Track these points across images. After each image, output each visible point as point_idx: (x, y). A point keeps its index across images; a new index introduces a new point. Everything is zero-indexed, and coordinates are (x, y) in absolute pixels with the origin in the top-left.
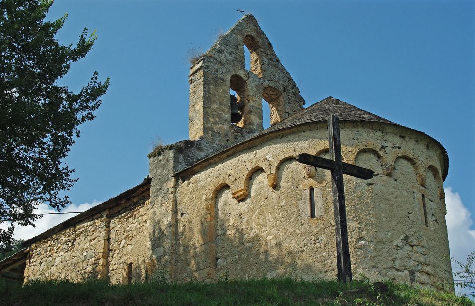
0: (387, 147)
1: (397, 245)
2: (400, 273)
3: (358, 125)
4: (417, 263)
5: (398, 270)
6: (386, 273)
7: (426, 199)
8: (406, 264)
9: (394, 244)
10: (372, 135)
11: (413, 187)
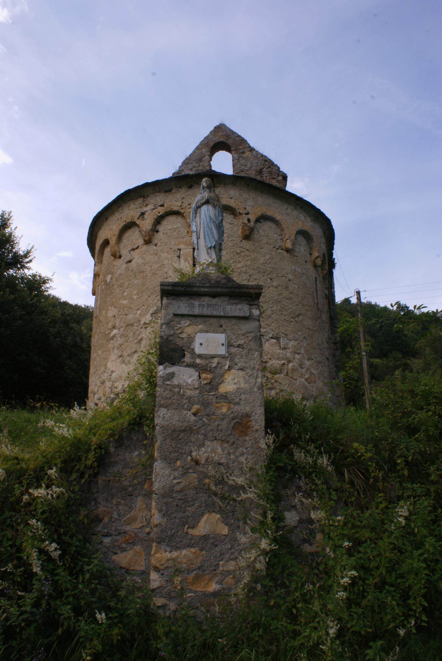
1: (145, 323)
9: (142, 323)
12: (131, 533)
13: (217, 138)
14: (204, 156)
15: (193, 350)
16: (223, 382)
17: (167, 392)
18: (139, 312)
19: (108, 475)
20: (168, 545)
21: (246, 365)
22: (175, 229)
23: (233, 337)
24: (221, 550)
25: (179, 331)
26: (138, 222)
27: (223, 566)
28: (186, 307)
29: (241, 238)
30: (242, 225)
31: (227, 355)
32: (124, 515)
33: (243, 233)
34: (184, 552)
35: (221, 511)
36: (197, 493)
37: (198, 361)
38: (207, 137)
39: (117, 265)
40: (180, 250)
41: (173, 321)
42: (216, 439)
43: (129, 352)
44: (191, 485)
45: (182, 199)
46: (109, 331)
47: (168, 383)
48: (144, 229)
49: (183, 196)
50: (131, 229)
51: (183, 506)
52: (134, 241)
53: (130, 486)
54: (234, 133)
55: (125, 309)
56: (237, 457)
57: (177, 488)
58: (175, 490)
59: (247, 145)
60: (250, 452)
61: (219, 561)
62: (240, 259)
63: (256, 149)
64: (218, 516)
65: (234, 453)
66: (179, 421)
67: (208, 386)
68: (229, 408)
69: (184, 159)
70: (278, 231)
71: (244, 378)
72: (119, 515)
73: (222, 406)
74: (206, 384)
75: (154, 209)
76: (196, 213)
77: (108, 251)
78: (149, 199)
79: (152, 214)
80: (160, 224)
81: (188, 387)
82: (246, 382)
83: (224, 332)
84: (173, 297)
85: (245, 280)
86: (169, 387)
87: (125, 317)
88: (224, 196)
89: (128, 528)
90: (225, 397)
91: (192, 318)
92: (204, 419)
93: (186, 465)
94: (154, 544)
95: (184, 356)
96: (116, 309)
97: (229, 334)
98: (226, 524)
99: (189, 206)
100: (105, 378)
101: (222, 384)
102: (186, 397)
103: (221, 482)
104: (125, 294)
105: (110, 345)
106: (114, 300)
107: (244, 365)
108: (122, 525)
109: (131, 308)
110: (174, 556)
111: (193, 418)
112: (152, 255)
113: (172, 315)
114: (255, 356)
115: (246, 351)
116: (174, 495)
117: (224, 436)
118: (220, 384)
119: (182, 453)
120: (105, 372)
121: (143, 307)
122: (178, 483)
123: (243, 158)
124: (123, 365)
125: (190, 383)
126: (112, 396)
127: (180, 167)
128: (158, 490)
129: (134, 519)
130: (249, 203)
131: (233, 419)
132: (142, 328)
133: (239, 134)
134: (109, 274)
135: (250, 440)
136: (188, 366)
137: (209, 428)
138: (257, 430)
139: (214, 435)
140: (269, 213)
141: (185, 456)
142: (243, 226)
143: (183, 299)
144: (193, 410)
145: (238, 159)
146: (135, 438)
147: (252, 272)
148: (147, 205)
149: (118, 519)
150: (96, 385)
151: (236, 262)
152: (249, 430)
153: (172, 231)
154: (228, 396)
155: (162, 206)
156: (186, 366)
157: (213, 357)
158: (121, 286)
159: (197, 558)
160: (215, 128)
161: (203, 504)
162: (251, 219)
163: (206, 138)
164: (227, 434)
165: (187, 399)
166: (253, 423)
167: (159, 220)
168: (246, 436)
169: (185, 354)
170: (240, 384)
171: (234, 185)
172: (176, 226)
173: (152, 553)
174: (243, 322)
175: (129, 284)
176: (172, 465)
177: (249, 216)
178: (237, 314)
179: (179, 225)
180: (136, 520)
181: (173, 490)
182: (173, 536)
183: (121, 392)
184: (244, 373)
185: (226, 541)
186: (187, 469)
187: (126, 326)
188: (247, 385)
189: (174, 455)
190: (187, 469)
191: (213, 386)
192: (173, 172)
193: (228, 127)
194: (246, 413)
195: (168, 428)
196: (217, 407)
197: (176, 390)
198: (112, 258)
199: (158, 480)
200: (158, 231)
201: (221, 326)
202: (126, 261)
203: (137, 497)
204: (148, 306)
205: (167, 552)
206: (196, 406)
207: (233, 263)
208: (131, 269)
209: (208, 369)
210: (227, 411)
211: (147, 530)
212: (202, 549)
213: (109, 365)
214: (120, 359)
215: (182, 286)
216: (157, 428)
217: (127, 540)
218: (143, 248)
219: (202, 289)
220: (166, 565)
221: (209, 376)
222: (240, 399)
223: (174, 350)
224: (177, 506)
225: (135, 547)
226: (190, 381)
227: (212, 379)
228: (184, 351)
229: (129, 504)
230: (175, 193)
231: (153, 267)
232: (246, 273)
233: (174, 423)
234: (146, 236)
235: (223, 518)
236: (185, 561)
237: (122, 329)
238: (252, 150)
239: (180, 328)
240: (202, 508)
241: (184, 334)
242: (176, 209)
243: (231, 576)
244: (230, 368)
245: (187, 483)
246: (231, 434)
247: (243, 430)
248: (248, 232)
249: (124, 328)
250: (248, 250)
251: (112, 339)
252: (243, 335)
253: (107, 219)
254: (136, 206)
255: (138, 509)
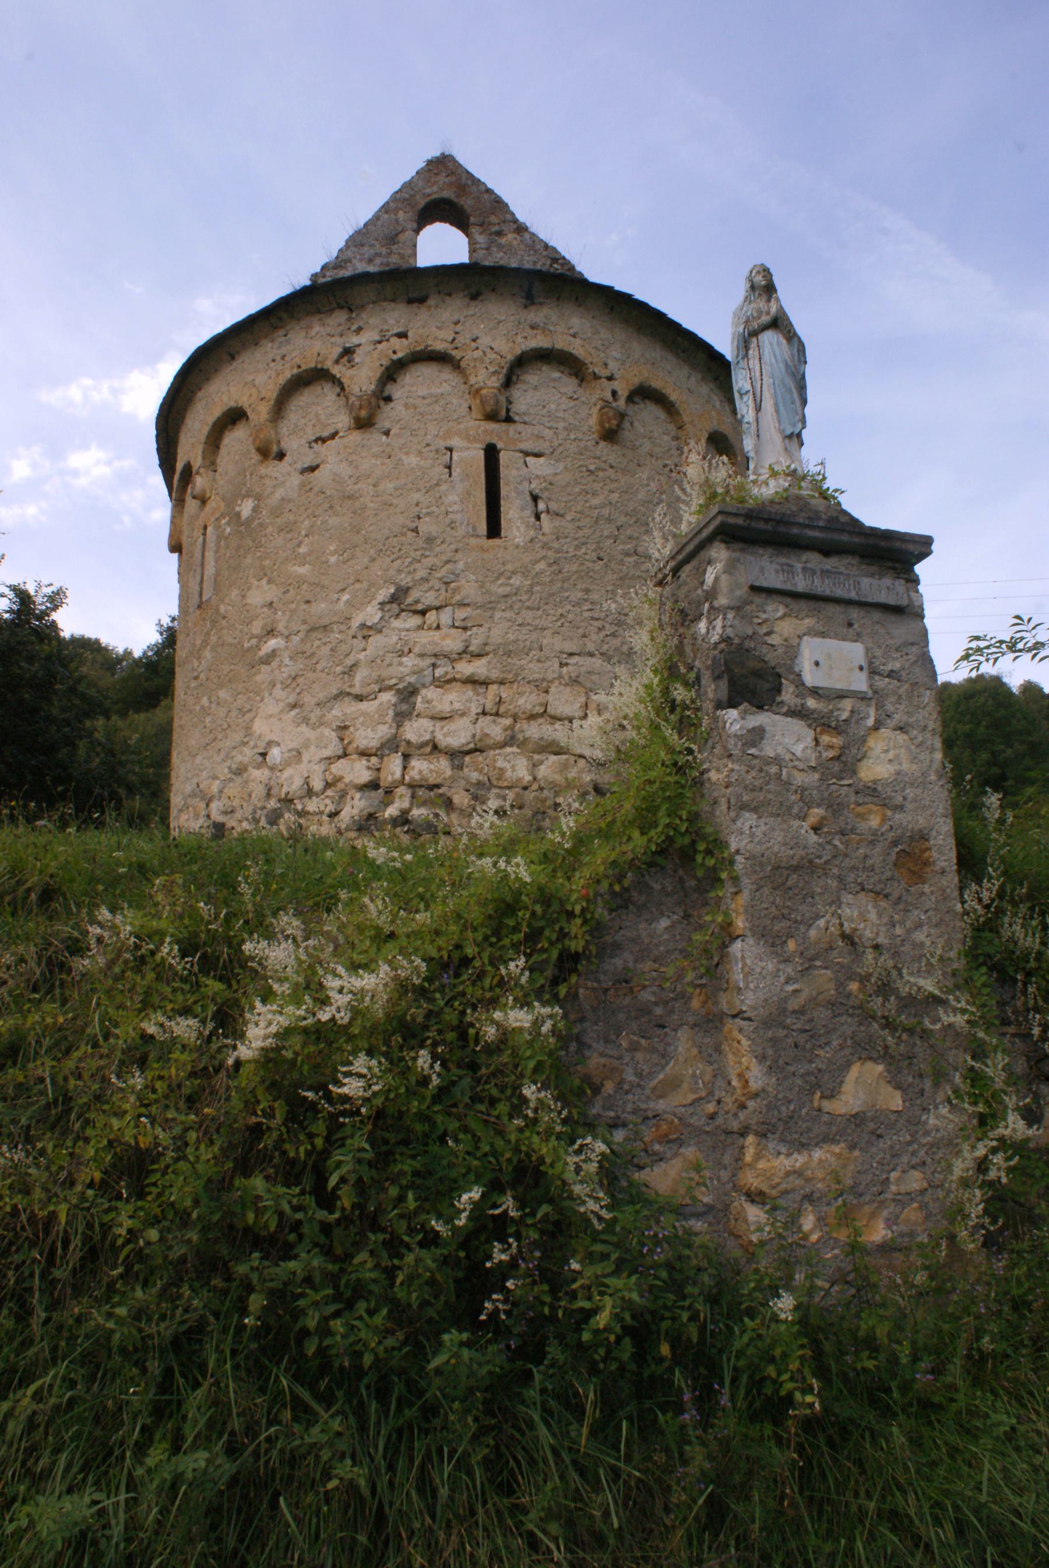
0: (359, 345)
1: (363, 626)
2: (364, 706)
3: (281, 319)
4: (429, 661)
5: (360, 698)
6: (324, 715)
7: (504, 457)
8: (385, 673)
9: (355, 624)
10: (317, 328)
11: (448, 435)
12: (670, 1117)
13: (435, 189)
14: (402, 231)
15: (799, 675)
16: (864, 757)
17: (753, 773)
18: (346, 597)
19: (602, 977)
20: (782, 1140)
21: (911, 720)
22: (437, 398)
23: (878, 653)
24: (891, 1147)
25: (764, 630)
26: (336, 371)
27: (899, 1180)
28: (777, 572)
29: (595, 436)
30: (600, 404)
31: (870, 694)
32: (651, 1075)
33: (601, 423)
34: (817, 1154)
35: (886, 1056)
36: (835, 1016)
37: (811, 703)
38: (410, 182)
39: (274, 475)
40: (450, 450)
41: (751, 603)
42: (863, 889)
43: (321, 696)
44: (821, 997)
45: (457, 323)
46: (254, 641)
47: (752, 751)
48: (356, 390)
49: (456, 318)
50: (311, 388)
51: (808, 1046)
52: (323, 417)
53: (656, 1004)
54: (477, 182)
55: (304, 587)
56: (909, 931)
57: (794, 1004)
58: (790, 1009)
59: (508, 217)
60: (934, 921)
61: (889, 1172)
62: (597, 486)
63: (533, 229)
64: (880, 1068)
65: (902, 922)
66: (785, 844)
67: (837, 763)
68: (884, 819)
69: (351, 232)
70: (672, 427)
71: (907, 748)
72: (639, 1075)
73: (870, 812)
74: (832, 759)
75: (380, 342)
76: (747, 348)
77: (237, 439)
78: (364, 316)
79: (375, 355)
80: (395, 381)
81: (796, 763)
82: (914, 759)
83: (857, 638)
84: (741, 545)
85: (608, 537)
86: (755, 762)
87: (304, 607)
88: (559, 329)
89: (661, 1105)
90: (871, 791)
91: (788, 600)
92: (837, 842)
93: (807, 949)
94: (750, 1139)
95: (779, 690)
96: (274, 587)
97: (870, 645)
98: (898, 1087)
99: (474, 345)
100: (246, 760)
101: (865, 762)
102: (794, 788)
103: (885, 989)
104: (303, 550)
105: (259, 678)
106: (267, 562)
107: (905, 718)
108: (648, 1098)
109: (323, 587)
110: (798, 1164)
111: (813, 838)
112: (375, 456)
113: (746, 589)
114: (926, 700)
115: (906, 686)
116: (788, 1021)
117: (880, 881)
118: (859, 760)
119: (796, 922)
120: (245, 744)
121: (358, 586)
122: (795, 991)
123: (500, 247)
124: (303, 728)
125: (799, 754)
126: (273, 804)
127: (341, 250)
128: (755, 1008)
129: (672, 1085)
130: (614, 354)
131: (895, 843)
132: (354, 637)
133: (490, 186)
134: (247, 496)
135: (932, 893)
136: (792, 713)
137: (848, 863)
138: (943, 872)
139: (859, 880)
140: (656, 384)
141: (802, 928)
142: (602, 408)
143: (761, 551)
144: (812, 820)
145: (487, 249)
146: (657, 886)
147: (622, 519)
148: (360, 329)
149: (639, 1085)
150: (215, 778)
151: (587, 493)
152: (928, 869)
153: (428, 401)
154: (879, 788)
155: (403, 335)
156: (786, 715)
157: (841, 695)
158: (289, 528)
159: (844, 1166)
160: (430, 163)
161: (849, 1042)
162: (620, 393)
163: (408, 185)
164: (884, 877)
165: (796, 792)
166: (935, 854)
167: (393, 372)
168: (923, 883)
169: (781, 684)
170: (900, 764)
171: (580, 306)
172: (439, 391)
173: (748, 1158)
174: (892, 618)
175: (312, 526)
176: (779, 949)
177: (616, 385)
178: (883, 598)
179: (446, 388)
180: (679, 1086)
181: (785, 1010)
182: (791, 1118)
183: (298, 794)
184: (906, 737)
185: (899, 1125)
186: (812, 959)
187: (309, 631)
188: (915, 766)
189: (780, 926)
190: (812, 959)
191: (845, 763)
192: (323, 263)
193: (460, 165)
194: (920, 831)
195: (764, 859)
196: (858, 815)
197: (774, 769)
198: (256, 457)
199: (752, 986)
200: (388, 399)
201: (850, 625)
202: (299, 466)
203: (675, 1030)
204: (372, 585)
205: (782, 1157)
206: (816, 810)
207: (580, 493)
208: (316, 489)
209: (833, 724)
210: (881, 825)
211: (711, 1108)
212: (852, 1147)
213: (260, 726)
214: (293, 713)
215: (767, 521)
216: (739, 859)
217: (666, 1135)
218: (351, 438)
219: (810, 533)
220: (783, 1186)
221: (835, 740)
222: (905, 798)
223: (757, 674)
224: (796, 1046)
225: (682, 1150)
226: (798, 749)
227: (843, 748)
228: (779, 676)
229: (661, 1049)
230: (437, 306)
231: (381, 487)
232: (609, 520)
233: (776, 848)
234: (361, 407)
235: (889, 1072)
236: (820, 1174)
237: (296, 639)
238: (521, 229)
239: (765, 621)
240: (847, 1051)
241: (773, 636)
242: (440, 346)
243: (915, 1205)
244: (876, 728)
245: (814, 993)
246: (892, 879)
247: (916, 869)
248: (615, 422)
249: (301, 635)
250: (612, 467)
251: (267, 660)
252: (897, 650)
253: (233, 357)
254: (328, 330)
255: (681, 1059)
